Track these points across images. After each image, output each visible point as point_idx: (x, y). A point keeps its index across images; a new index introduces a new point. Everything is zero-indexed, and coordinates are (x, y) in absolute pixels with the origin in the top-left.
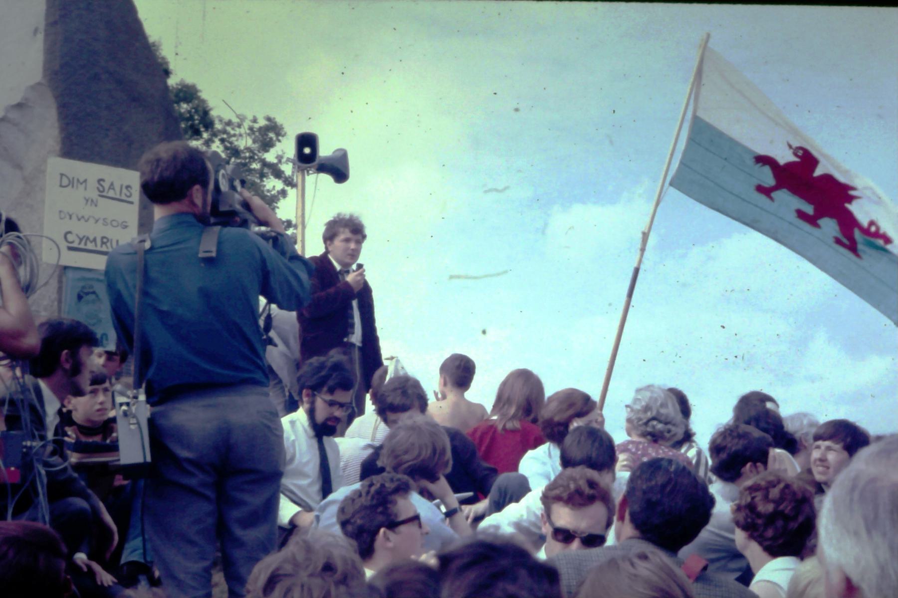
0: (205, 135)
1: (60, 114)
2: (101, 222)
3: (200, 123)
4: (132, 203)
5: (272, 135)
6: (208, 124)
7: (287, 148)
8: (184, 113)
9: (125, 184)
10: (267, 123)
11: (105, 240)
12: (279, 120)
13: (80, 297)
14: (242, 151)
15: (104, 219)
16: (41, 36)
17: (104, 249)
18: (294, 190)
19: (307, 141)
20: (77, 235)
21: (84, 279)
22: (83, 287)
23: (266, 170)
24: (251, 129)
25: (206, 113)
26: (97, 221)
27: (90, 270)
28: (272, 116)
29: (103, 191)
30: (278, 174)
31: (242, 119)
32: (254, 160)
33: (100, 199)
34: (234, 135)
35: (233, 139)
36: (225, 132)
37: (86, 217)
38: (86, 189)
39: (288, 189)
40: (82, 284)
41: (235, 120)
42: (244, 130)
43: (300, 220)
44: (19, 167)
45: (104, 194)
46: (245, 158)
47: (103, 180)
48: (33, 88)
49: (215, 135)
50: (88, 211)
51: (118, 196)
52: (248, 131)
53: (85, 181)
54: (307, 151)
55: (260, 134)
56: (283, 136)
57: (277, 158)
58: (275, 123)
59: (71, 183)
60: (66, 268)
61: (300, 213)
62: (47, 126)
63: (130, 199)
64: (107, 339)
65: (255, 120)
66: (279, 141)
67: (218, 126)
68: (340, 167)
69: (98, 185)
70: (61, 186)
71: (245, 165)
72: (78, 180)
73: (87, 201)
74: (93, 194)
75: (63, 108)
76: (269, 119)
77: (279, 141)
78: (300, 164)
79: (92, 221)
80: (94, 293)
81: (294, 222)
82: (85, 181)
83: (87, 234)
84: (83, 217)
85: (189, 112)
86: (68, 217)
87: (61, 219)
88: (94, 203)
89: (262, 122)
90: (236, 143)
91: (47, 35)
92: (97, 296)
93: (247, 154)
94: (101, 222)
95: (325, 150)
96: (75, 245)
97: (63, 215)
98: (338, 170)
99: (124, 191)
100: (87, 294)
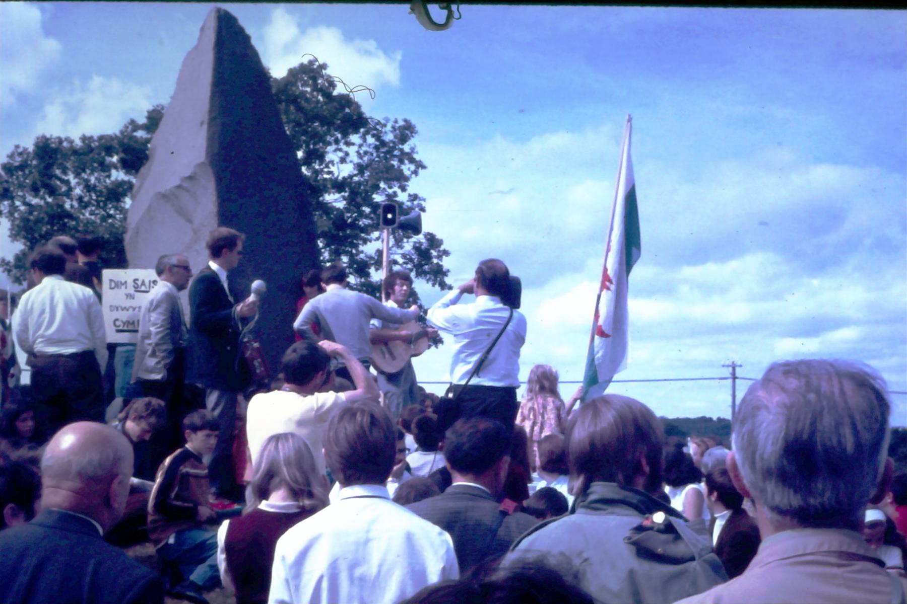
5: (407, 132)
12: (414, 121)
16: (205, 127)
24: (393, 127)
28: (408, 118)
31: (387, 120)
36: (376, 129)
40: (126, 355)
41: (383, 122)
42: (389, 128)
44: (190, 221)
47: (137, 280)
53: (126, 282)
65: (396, 122)
67: (372, 125)
74: (131, 290)
75: (219, 180)
76: (405, 121)
79: (131, 310)
82: (126, 282)
96: (121, 328)
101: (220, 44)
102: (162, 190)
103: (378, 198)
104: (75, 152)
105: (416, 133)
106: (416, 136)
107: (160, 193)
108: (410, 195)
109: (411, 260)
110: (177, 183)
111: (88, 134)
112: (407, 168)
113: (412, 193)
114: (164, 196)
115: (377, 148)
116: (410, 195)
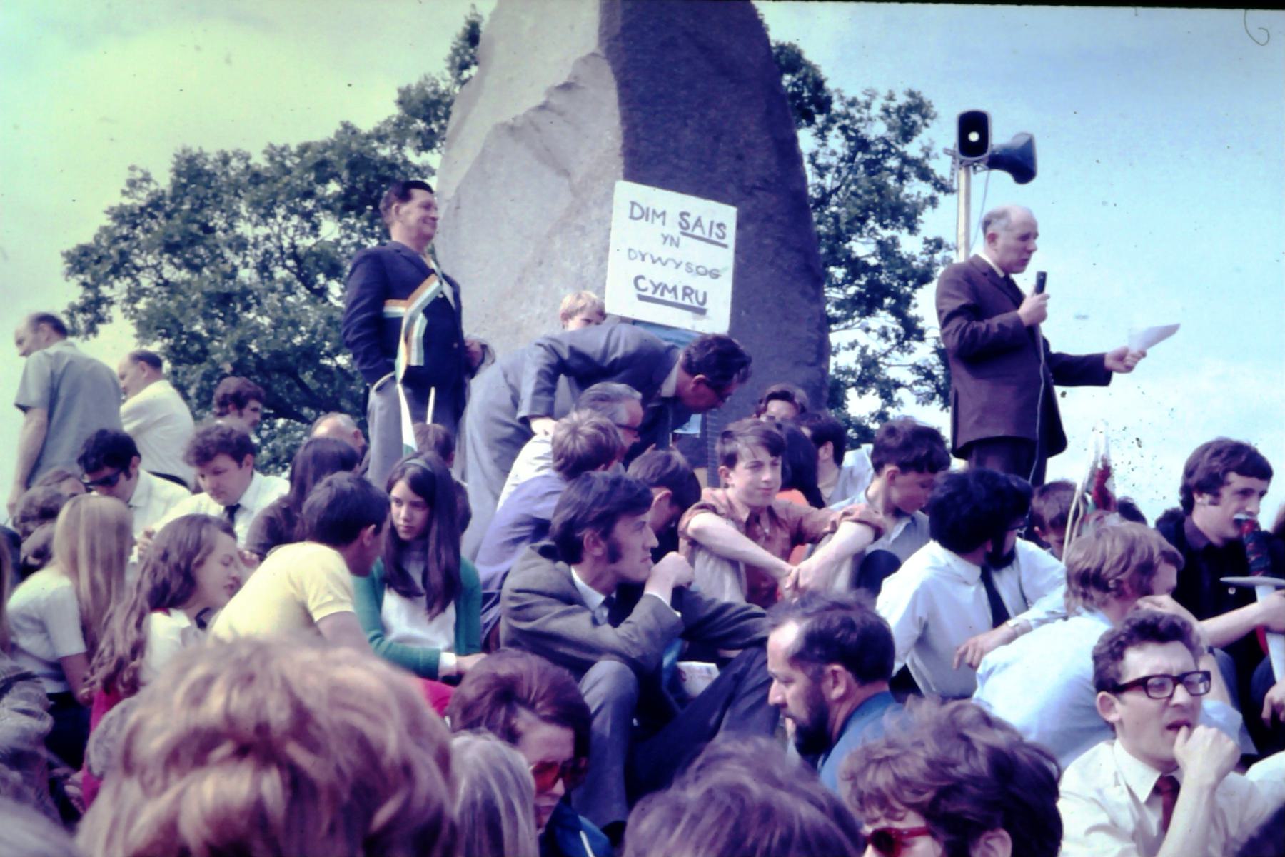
0: (819, 119)
2: (683, 266)
4: (725, 246)
5: (915, 117)
6: (824, 104)
7: (939, 138)
9: (717, 221)
10: (909, 100)
12: (927, 95)
14: (872, 143)
15: (688, 264)
17: (687, 302)
18: (950, 197)
19: (973, 122)
20: (652, 282)
23: (906, 169)
24: (886, 110)
25: (818, 84)
26: (678, 266)
28: (916, 89)
29: (688, 227)
30: (925, 174)
34: (861, 120)
36: (847, 116)
37: (664, 260)
38: (664, 223)
39: (941, 196)
41: (862, 98)
42: (876, 110)
43: (962, 240)
44: (567, 173)
45: (689, 231)
46: (877, 153)
47: (688, 214)
48: (584, 61)
49: (831, 120)
50: (666, 252)
51: (707, 236)
52: (882, 114)
53: (664, 213)
54: (974, 137)
55: (898, 115)
56: (932, 119)
57: (923, 150)
58: (921, 99)
59: (645, 214)
61: (962, 230)
63: (723, 241)
65: (891, 98)
66: (927, 125)
67: (837, 107)
69: (679, 219)
70: (632, 217)
71: (877, 162)
72: (654, 212)
73: (666, 239)
74: (675, 231)
75: (625, 87)
76: (912, 94)
77: (927, 125)
78: (963, 158)
79: (671, 265)
82: (664, 213)
83: (665, 281)
84: (660, 259)
85: (794, 85)
86: (639, 257)
89: (902, 100)
90: (863, 131)
94: (683, 266)
95: (1000, 137)
96: (649, 294)
97: (633, 255)
98: (1020, 165)
99: (715, 230)
102: (507, 117)
104: (256, 178)
107: (503, 125)
108: (927, 241)
109: (929, 376)
110: (541, 99)
111: (279, 143)
112: (916, 189)
113: (930, 237)
114: (512, 130)
116: (927, 241)
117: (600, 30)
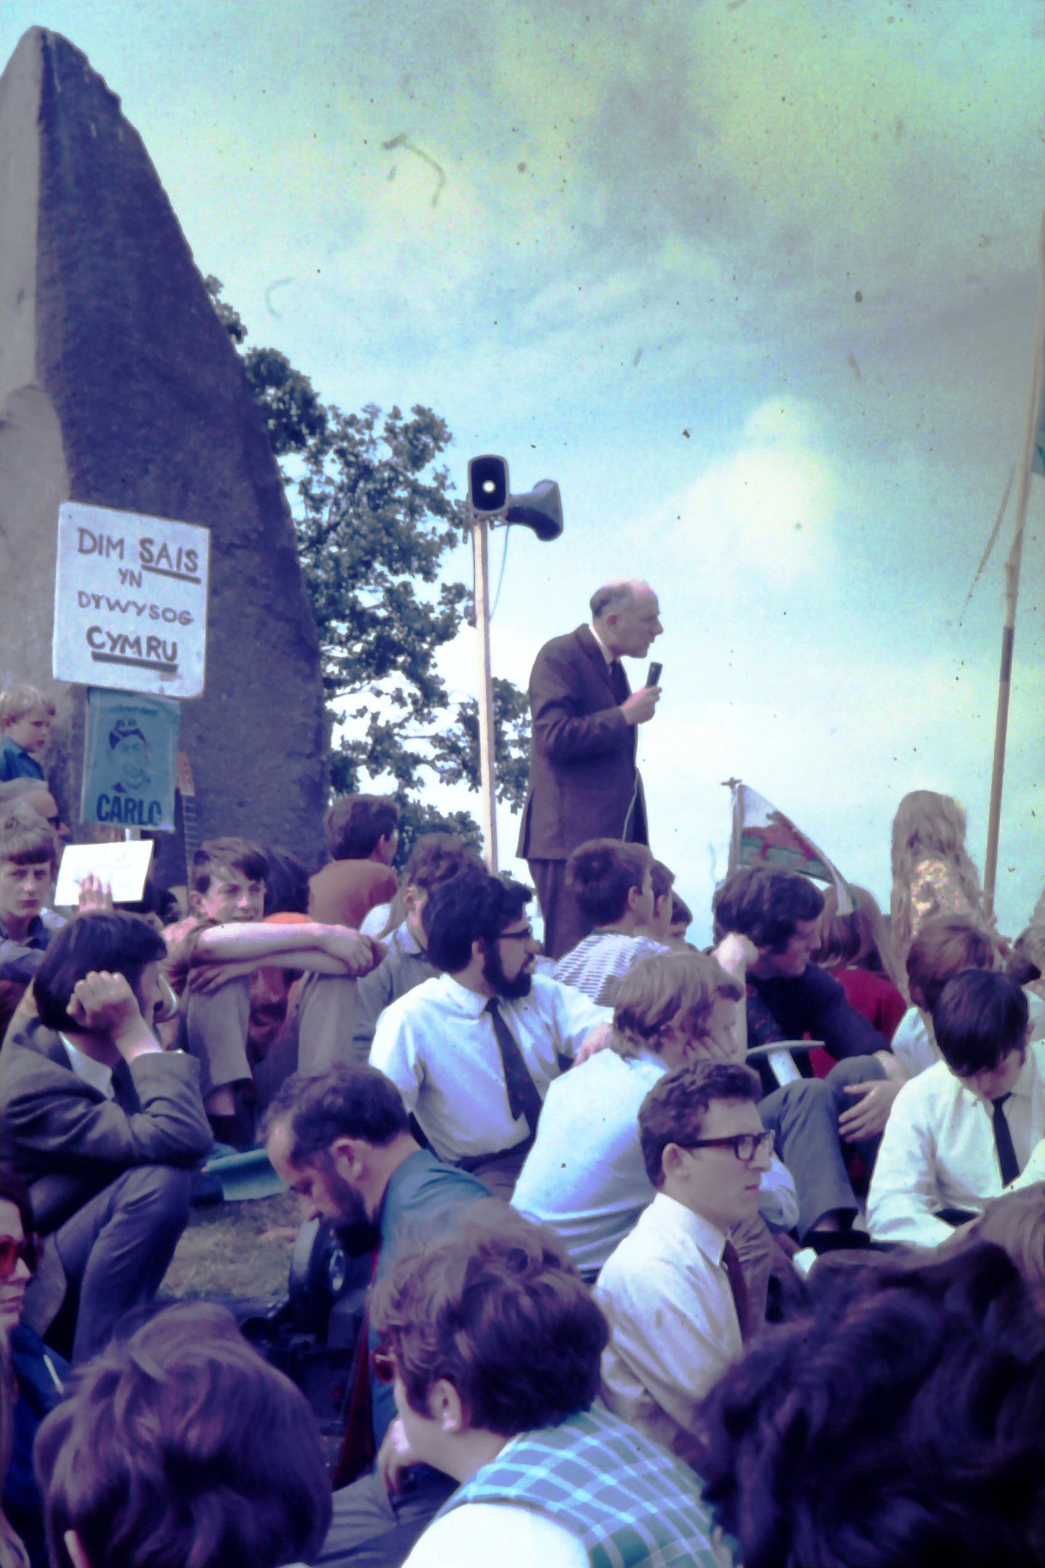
0: (311, 442)
1: (66, 437)
2: (147, 612)
3: (300, 422)
4: (197, 581)
5: (426, 439)
6: (316, 423)
8: (270, 409)
9: (187, 547)
11: (154, 643)
13: (113, 740)
14: (378, 469)
16: (29, 304)
17: (153, 657)
19: (488, 469)
20: (109, 635)
21: (121, 709)
22: (120, 723)
23: (418, 501)
24: (390, 429)
25: (308, 401)
26: (140, 611)
27: (130, 694)
28: (426, 405)
29: (151, 560)
31: (373, 411)
32: (399, 483)
33: (145, 574)
34: (362, 442)
35: (362, 449)
36: (345, 437)
37: (123, 603)
38: (121, 556)
40: (114, 717)
41: (362, 416)
42: (379, 430)
45: (153, 565)
46: (383, 481)
47: (150, 541)
49: (325, 442)
50: (128, 593)
51: (175, 569)
52: (385, 434)
53: (121, 542)
54: (489, 487)
55: (406, 436)
58: (432, 417)
60: (90, 690)
62: (45, 444)
64: (159, 812)
65: (396, 414)
66: (440, 449)
67: (332, 426)
68: (550, 514)
69: (140, 549)
71: (382, 492)
72: (109, 541)
76: (419, 410)
77: (440, 449)
79: (132, 610)
80: (137, 732)
81: (469, 586)
82: (121, 542)
85: (280, 400)
87: (82, 605)
88: (137, 581)
89: (409, 418)
90: (365, 456)
91: (40, 301)
92: (142, 737)
93: (386, 474)
94: (147, 612)
95: (520, 484)
96: (106, 650)
99: (184, 560)
100: (125, 734)
101: (48, 114)
103: (368, 597)
105: (449, 438)
106: (448, 448)
115: (351, 488)
117: (38, 353)
